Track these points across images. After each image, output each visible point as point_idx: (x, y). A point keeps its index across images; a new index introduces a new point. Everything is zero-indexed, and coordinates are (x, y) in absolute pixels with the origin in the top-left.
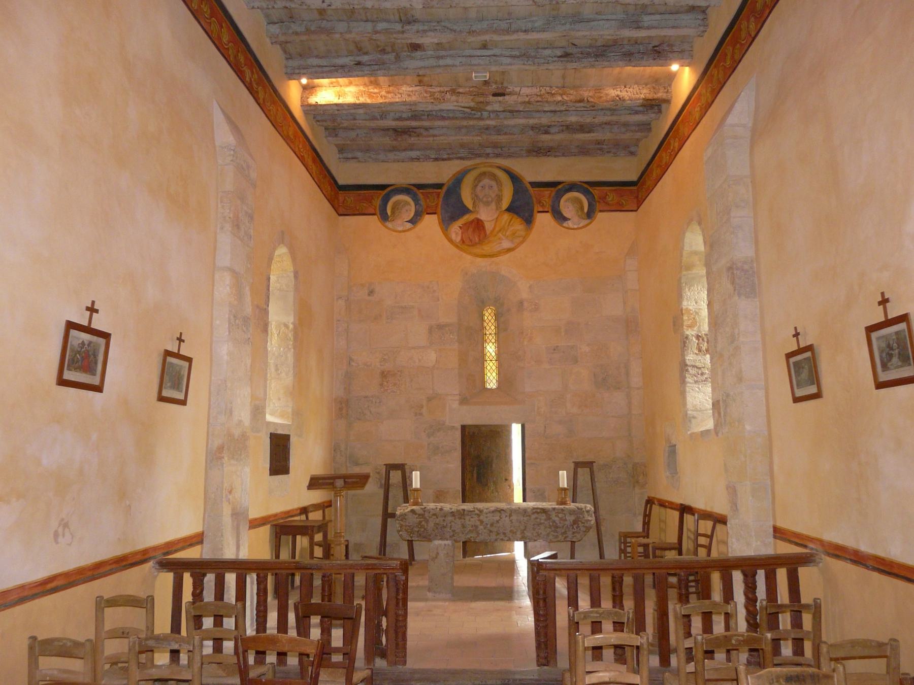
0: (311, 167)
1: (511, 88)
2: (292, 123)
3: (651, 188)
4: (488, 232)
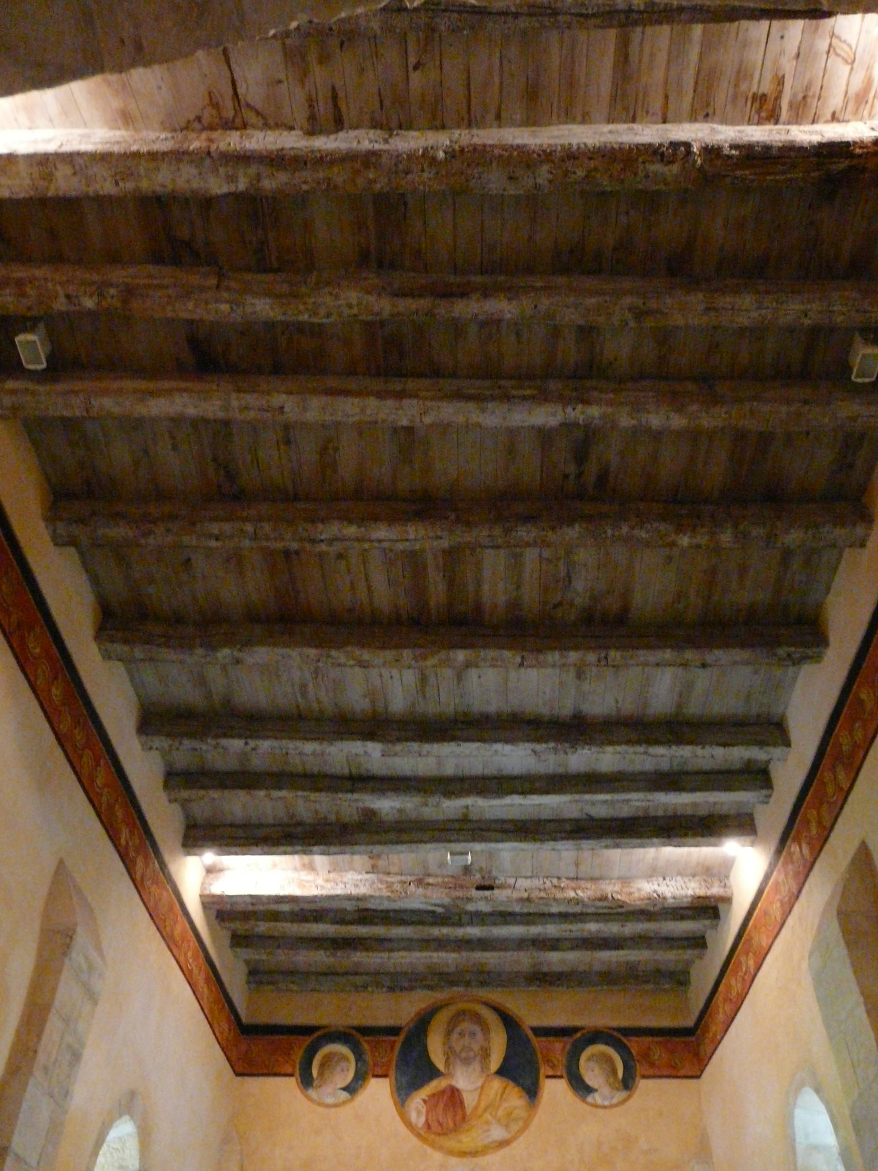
0: (201, 990)
1: (501, 880)
2: (181, 919)
3: (719, 1037)
4: (469, 1111)
